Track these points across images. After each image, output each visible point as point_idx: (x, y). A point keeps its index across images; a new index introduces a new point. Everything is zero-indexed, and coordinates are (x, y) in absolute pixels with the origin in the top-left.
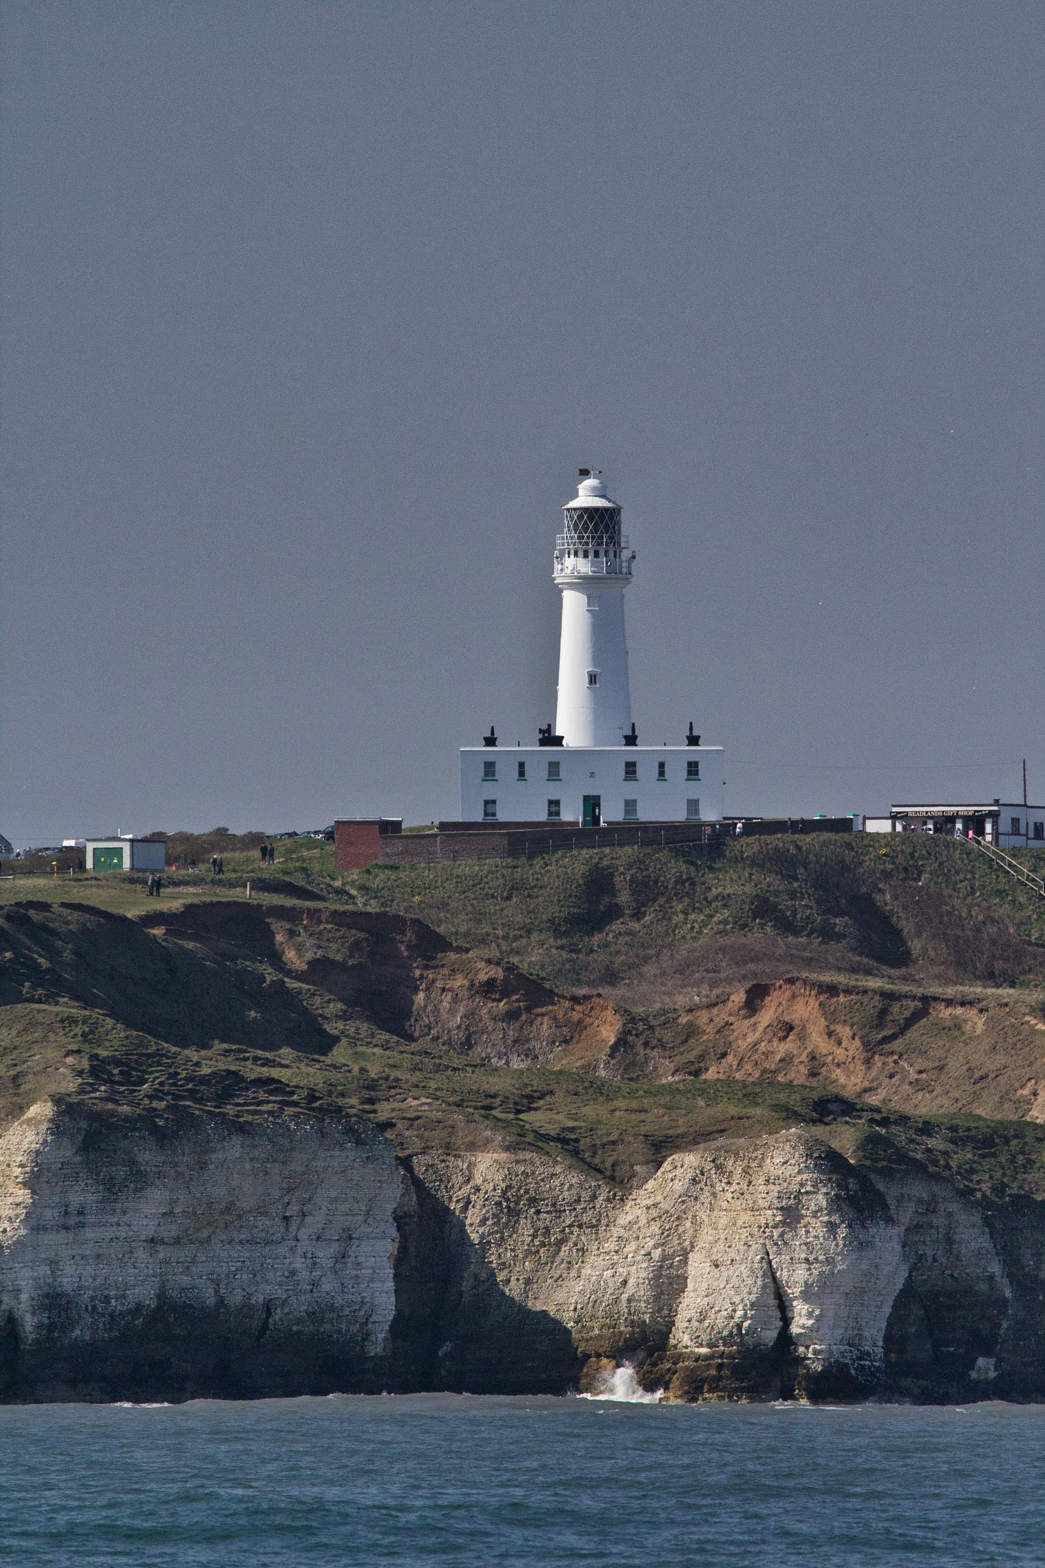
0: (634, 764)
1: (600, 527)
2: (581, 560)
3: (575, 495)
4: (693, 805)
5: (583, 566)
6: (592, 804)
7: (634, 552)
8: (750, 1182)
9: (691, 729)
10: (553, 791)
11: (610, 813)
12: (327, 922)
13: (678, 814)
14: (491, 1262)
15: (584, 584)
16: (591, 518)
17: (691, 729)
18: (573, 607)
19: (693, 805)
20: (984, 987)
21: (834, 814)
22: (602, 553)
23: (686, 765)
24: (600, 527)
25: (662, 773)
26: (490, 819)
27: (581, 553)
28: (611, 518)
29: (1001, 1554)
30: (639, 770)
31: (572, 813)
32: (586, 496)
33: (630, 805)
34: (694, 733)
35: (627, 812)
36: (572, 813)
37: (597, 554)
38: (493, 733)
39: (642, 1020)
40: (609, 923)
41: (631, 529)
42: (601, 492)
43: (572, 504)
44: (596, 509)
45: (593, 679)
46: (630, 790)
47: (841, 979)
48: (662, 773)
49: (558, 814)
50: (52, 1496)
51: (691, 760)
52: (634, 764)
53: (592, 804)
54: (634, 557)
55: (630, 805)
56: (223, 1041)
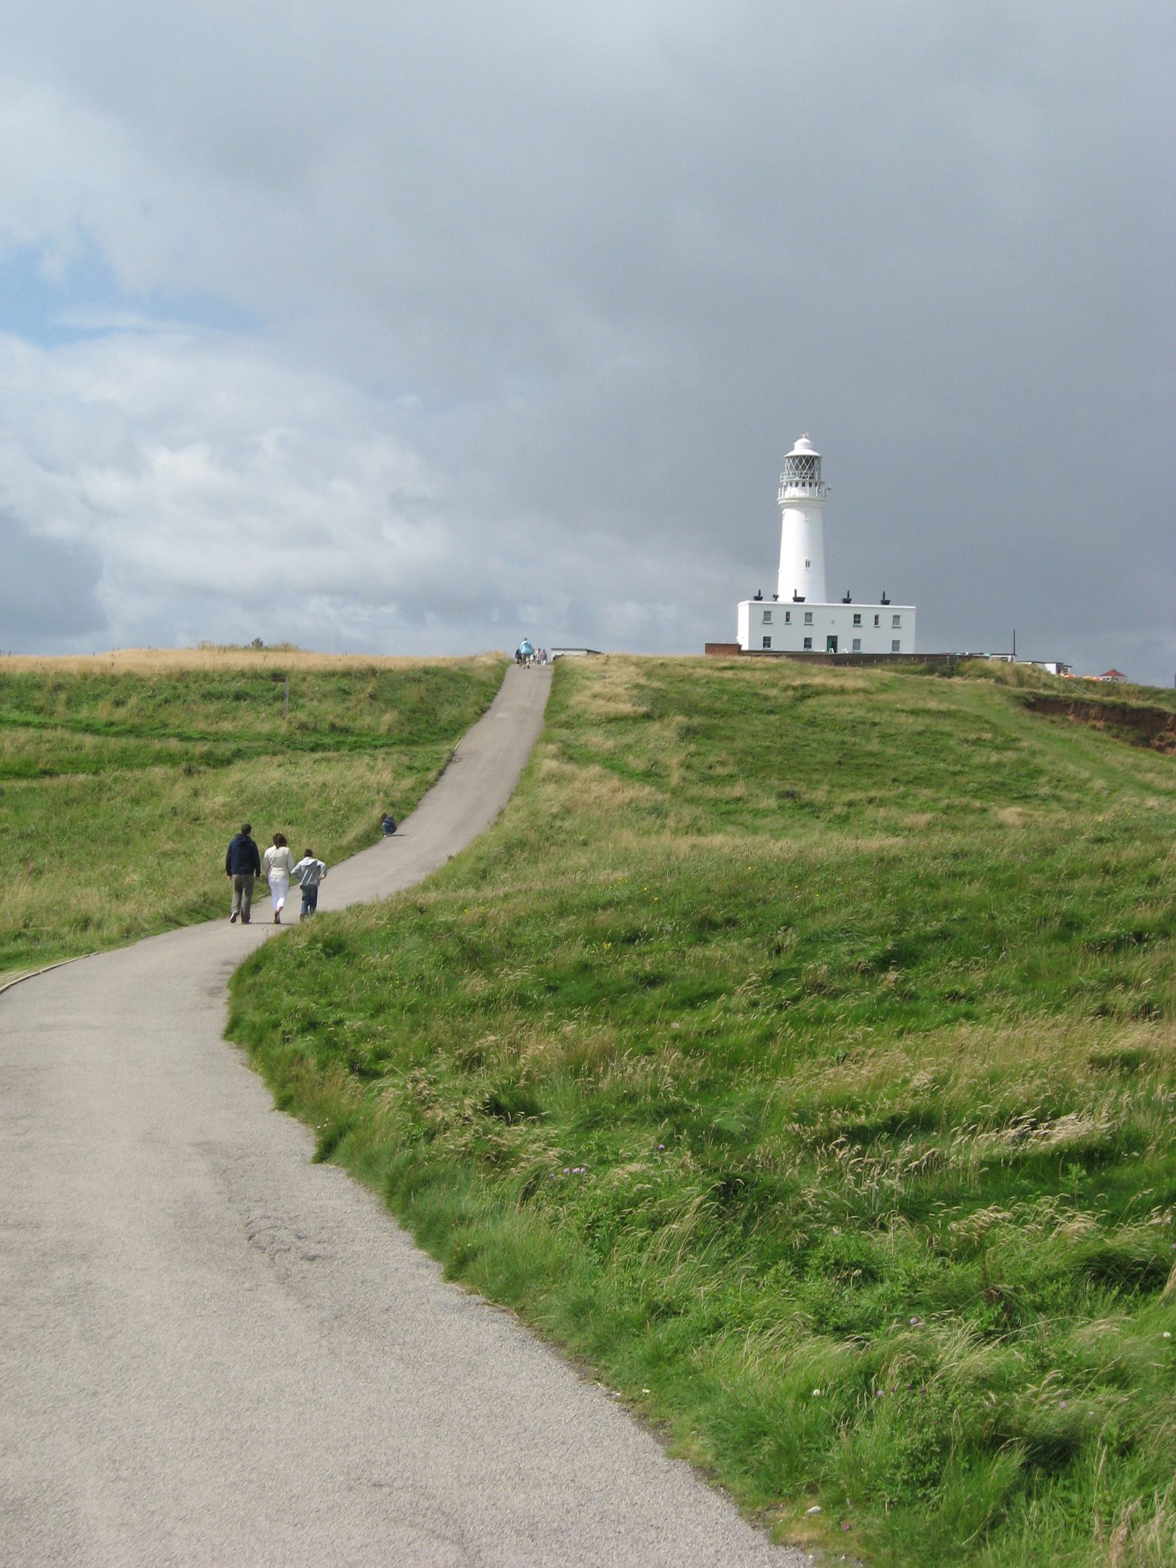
0: (769, 613)
3: (792, 449)
4: (896, 644)
6: (832, 642)
10: (896, 635)
11: (844, 648)
12: (1095, 718)
25: (788, 620)
26: (767, 649)
27: (800, 484)
28: (816, 462)
31: (820, 647)
32: (801, 448)
33: (857, 643)
35: (854, 647)
36: (820, 647)
37: (804, 485)
40: (1053, 713)
43: (790, 454)
45: (808, 564)
46: (857, 633)
48: (788, 620)
49: (810, 646)
50: (347, 1522)
52: (769, 613)
53: (832, 642)
55: (857, 643)
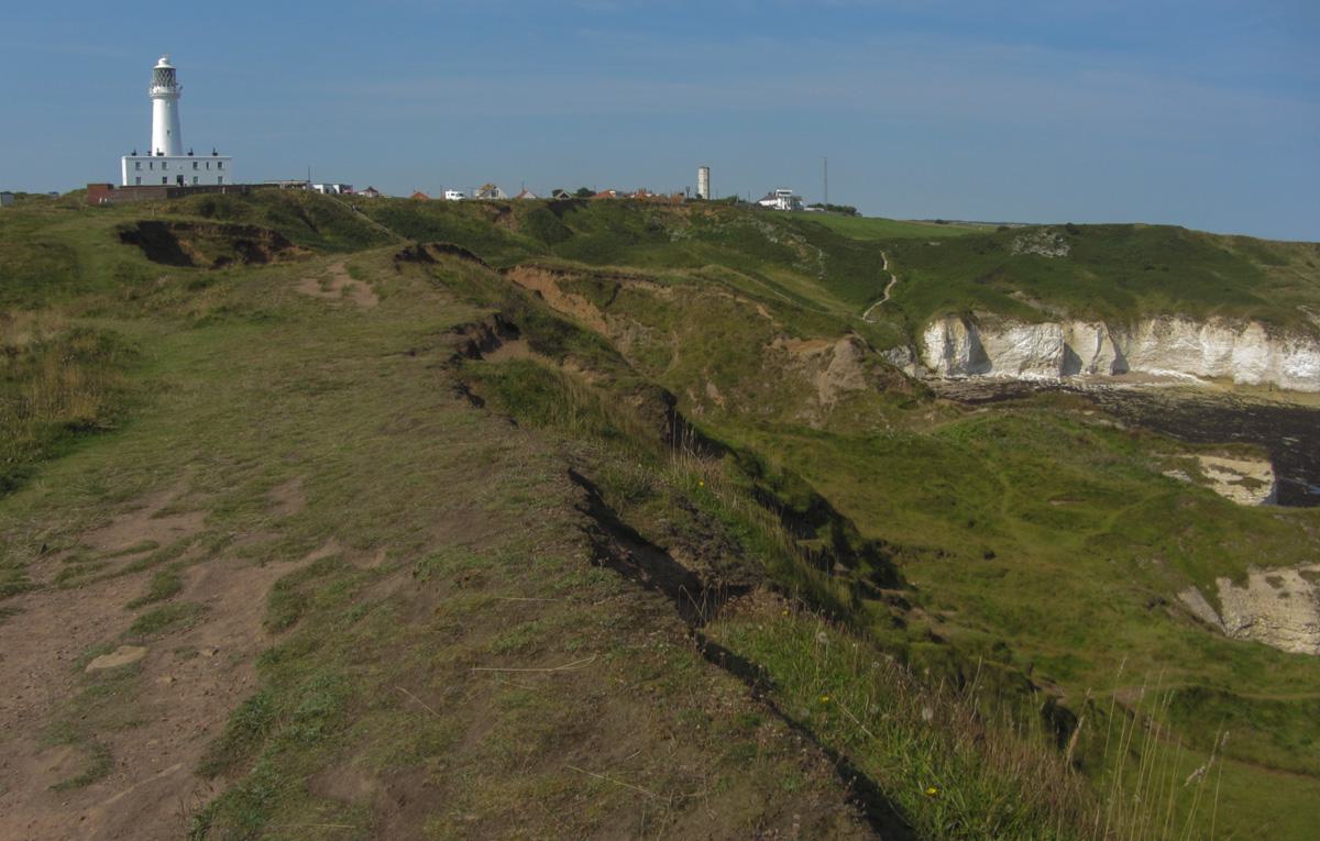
1: (168, 76)
4: (220, 178)
6: (180, 179)
8: (1060, 722)
10: (220, 173)
13: (215, 182)
14: (544, 473)
18: (159, 109)
19: (220, 178)
20: (1153, 388)
21: (849, 205)
24: (168, 76)
32: (161, 64)
33: (195, 179)
39: (1242, 326)
41: (179, 77)
42: (167, 62)
45: (168, 132)
47: (567, 263)
53: (180, 179)
56: (895, 284)
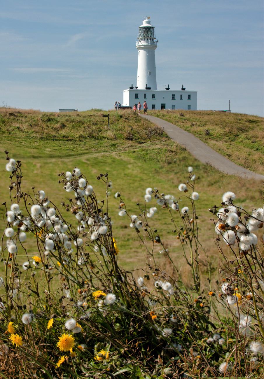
1: (148, 31)
2: (143, 41)
5: (143, 43)
7: (158, 40)
9: (183, 87)
15: (143, 48)
16: (146, 29)
17: (183, 87)
22: (149, 39)
23: (152, 95)
25: (145, 97)
27: (143, 39)
29: (16, 310)
30: (139, 96)
34: (184, 88)
37: (147, 40)
38: (168, 87)
41: (157, 33)
44: (147, 27)
51: (189, 94)
54: (158, 41)
